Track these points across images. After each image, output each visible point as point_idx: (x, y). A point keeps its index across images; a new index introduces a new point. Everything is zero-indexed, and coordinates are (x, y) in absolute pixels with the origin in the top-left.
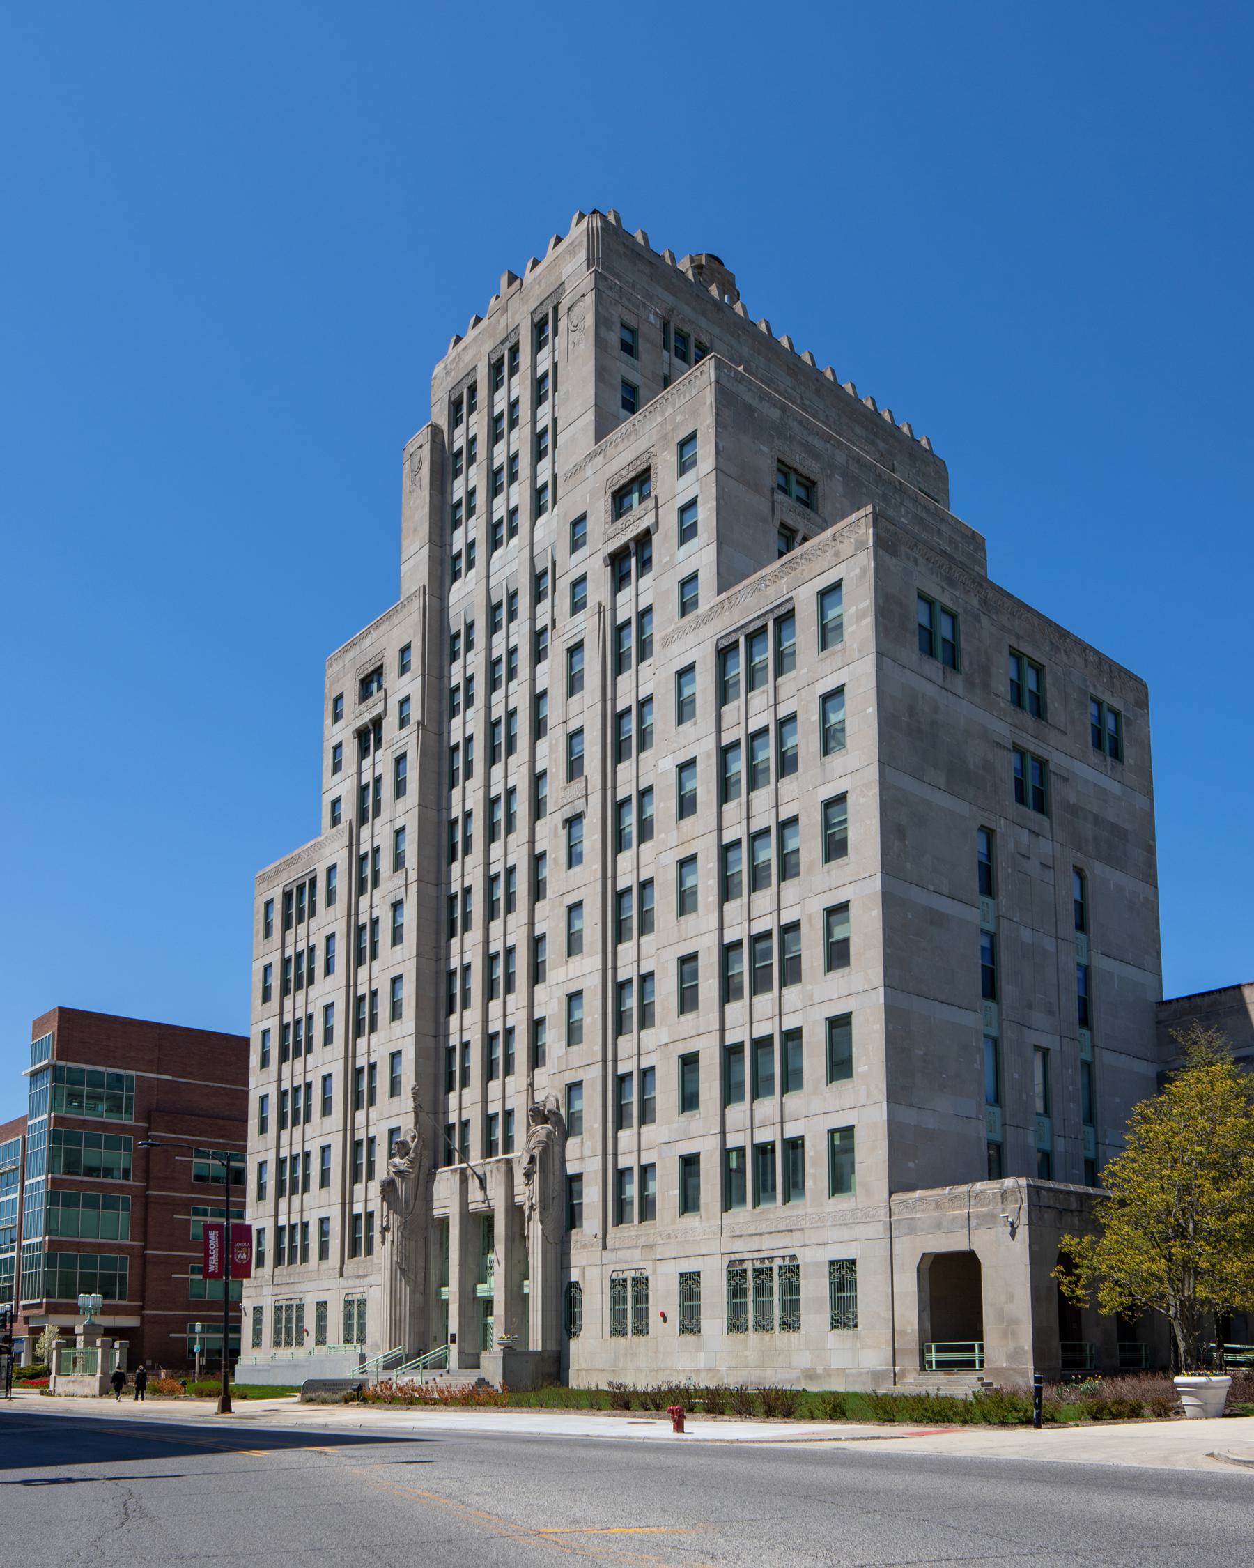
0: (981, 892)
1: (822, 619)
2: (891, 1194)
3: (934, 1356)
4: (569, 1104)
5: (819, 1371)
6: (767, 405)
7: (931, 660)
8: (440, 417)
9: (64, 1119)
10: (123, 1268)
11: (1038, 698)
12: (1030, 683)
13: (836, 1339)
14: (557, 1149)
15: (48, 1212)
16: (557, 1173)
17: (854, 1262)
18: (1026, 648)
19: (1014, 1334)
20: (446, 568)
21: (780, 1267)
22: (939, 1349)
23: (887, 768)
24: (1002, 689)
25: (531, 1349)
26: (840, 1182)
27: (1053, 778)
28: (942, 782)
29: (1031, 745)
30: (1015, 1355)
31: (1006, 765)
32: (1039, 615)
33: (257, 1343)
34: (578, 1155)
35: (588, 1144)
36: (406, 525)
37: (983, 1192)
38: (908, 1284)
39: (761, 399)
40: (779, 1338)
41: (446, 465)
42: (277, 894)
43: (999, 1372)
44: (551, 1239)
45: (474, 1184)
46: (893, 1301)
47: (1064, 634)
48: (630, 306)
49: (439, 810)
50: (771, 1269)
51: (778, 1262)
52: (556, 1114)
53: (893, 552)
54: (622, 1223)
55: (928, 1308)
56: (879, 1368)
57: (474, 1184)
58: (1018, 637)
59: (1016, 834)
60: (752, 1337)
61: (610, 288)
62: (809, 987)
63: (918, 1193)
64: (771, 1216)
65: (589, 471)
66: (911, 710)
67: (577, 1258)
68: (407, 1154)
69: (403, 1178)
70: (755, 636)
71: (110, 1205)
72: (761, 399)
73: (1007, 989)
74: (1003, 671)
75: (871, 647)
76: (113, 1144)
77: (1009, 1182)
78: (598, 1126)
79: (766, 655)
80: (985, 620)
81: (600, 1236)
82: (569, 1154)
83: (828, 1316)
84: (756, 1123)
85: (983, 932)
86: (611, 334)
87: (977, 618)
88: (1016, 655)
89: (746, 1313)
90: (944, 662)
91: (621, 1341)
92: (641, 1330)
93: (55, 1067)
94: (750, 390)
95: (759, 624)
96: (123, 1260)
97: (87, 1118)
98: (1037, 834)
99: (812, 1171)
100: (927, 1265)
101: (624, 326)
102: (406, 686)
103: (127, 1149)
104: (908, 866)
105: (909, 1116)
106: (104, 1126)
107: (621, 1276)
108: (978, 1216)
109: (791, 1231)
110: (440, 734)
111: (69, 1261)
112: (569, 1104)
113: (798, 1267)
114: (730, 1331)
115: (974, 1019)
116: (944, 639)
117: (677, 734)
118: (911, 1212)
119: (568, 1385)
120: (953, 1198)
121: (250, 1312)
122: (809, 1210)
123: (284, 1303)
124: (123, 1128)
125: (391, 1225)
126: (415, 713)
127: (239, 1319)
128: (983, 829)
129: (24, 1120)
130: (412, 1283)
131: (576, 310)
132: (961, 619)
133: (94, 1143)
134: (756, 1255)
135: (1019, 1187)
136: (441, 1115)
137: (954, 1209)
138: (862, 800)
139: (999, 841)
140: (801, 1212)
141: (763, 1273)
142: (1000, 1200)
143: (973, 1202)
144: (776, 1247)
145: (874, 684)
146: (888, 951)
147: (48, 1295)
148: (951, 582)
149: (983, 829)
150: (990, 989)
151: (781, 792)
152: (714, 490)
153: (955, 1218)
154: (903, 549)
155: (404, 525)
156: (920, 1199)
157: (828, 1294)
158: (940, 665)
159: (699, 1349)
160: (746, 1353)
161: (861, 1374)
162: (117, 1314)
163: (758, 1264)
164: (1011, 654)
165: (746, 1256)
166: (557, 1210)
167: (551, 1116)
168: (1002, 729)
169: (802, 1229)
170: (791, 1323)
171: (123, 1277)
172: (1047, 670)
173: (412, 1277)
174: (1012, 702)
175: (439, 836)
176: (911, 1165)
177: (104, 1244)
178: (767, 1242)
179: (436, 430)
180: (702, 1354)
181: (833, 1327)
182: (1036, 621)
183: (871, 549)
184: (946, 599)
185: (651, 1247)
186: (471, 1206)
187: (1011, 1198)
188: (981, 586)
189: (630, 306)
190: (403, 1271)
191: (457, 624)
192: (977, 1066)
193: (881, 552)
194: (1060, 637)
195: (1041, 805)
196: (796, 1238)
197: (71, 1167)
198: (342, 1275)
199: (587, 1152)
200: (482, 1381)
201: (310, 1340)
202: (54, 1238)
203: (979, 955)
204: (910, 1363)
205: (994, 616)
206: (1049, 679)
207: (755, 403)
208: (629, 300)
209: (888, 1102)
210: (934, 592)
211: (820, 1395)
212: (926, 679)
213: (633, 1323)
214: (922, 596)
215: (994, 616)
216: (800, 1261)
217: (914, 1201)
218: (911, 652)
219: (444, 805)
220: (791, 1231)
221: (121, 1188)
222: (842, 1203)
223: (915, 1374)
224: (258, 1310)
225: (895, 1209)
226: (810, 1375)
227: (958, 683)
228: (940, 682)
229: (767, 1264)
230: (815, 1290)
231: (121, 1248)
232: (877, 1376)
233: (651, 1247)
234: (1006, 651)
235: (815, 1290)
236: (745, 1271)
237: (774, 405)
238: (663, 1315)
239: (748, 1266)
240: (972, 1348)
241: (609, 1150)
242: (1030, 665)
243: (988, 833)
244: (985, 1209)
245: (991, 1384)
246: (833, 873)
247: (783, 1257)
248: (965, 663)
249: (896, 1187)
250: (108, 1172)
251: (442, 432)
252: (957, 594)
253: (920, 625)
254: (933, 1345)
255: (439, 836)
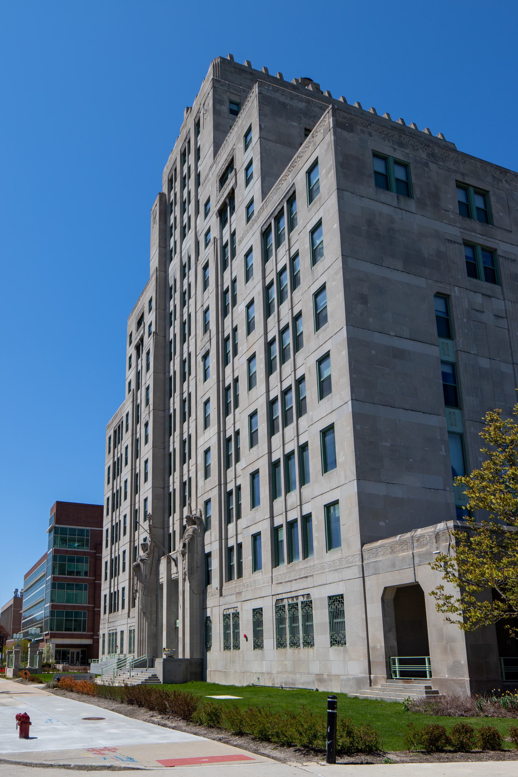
0: (440, 335)
1: (310, 185)
2: (362, 545)
3: (397, 667)
4: (206, 513)
5: (325, 677)
6: (296, 101)
7: (387, 192)
8: (165, 190)
9: (58, 550)
10: (84, 617)
11: (485, 212)
12: (478, 202)
13: (334, 652)
14: (199, 539)
15: (52, 592)
16: (200, 553)
17: (342, 596)
18: (468, 180)
19: (452, 651)
20: (166, 256)
21: (302, 602)
22: (401, 662)
23: (349, 260)
24: (451, 207)
25: (186, 658)
26: (332, 541)
27: (501, 260)
28: (399, 265)
29: (480, 240)
30: (454, 668)
31: (459, 256)
32: (481, 161)
33: (103, 653)
34: (209, 542)
35: (213, 534)
36: (152, 243)
37: (422, 536)
38: (376, 611)
39: (292, 99)
40: (303, 652)
41: (166, 209)
42: (112, 433)
43: (442, 682)
44: (195, 592)
45: (173, 564)
46: (368, 624)
47: (504, 171)
48: (235, 92)
49: (165, 374)
50: (297, 604)
51: (301, 599)
52: (200, 519)
53: (350, 129)
54: (231, 580)
55: (394, 630)
56: (360, 675)
57: (173, 564)
58: (463, 174)
59: (467, 297)
60: (289, 650)
61: (222, 85)
62: (311, 413)
63: (380, 542)
64: (297, 568)
65: (210, 175)
66: (370, 223)
67: (210, 602)
68: (147, 550)
69: (144, 563)
70: (278, 218)
71: (79, 587)
72: (292, 99)
73: (468, 400)
74: (452, 197)
75: (335, 187)
76: (79, 560)
77: (441, 526)
78: (217, 523)
79: (285, 222)
80: (433, 167)
81: (219, 588)
82: (206, 541)
83: (328, 636)
84: (289, 508)
85: (443, 362)
86: (223, 107)
87: (426, 165)
88: (462, 186)
89: (286, 635)
90: (398, 192)
91: (227, 652)
92: (237, 647)
93: (55, 527)
94: (283, 95)
95: (280, 207)
96: (85, 613)
97: (69, 549)
98: (489, 297)
99: (317, 535)
100: (391, 596)
101: (231, 102)
102: (150, 318)
103: (87, 562)
104: (371, 320)
105: (380, 489)
106: (76, 553)
107: (228, 613)
108: (420, 555)
109: (306, 577)
110: (165, 337)
111: (60, 614)
112: (206, 513)
113: (311, 601)
114: (278, 647)
115: (440, 421)
116: (397, 180)
117: (246, 288)
118: (375, 557)
119: (206, 681)
120: (402, 543)
121: (101, 636)
122: (316, 562)
123: (111, 632)
124: (85, 553)
125: (138, 589)
126: (153, 329)
127: (98, 639)
128: (438, 295)
129: (47, 553)
130: (149, 620)
131: (206, 103)
132: (412, 167)
133: (71, 560)
134: (289, 595)
135: (448, 528)
136: (166, 529)
137: (403, 551)
138: (334, 283)
139: (454, 301)
140: (311, 564)
141: (293, 607)
142: (434, 541)
143: (415, 544)
144: (298, 588)
145: (337, 208)
146: (355, 376)
147: (51, 630)
148: (401, 145)
149: (438, 295)
150: (452, 397)
151: (294, 299)
152: (259, 149)
153: (404, 558)
154: (359, 128)
155: (151, 243)
156: (380, 547)
157: (328, 621)
158: (394, 195)
159: (263, 659)
160: (286, 662)
161: (349, 680)
162: (81, 638)
163: (290, 601)
164: (458, 186)
165: (284, 596)
166: (199, 575)
167: (196, 520)
168: (454, 230)
169: (312, 576)
170: (309, 643)
171: (85, 621)
172: (491, 193)
173: (149, 616)
174: (461, 214)
175: (165, 386)
176: (382, 524)
177: (76, 606)
178: (295, 586)
179: (162, 195)
180: (264, 662)
181: (332, 644)
182: (479, 164)
183: (332, 130)
184: (399, 155)
185: (240, 593)
186: (173, 576)
187: (443, 538)
188: (429, 146)
189: (235, 92)
190: (144, 613)
191: (171, 282)
192: (443, 453)
193: (339, 130)
194: (501, 173)
195: (492, 277)
196: (308, 583)
197: (62, 572)
198: (129, 617)
199: (213, 539)
200: (155, 676)
201: (322, 635)
202: (53, 603)
203: (441, 377)
204: (380, 672)
205: (441, 163)
206: (493, 199)
207: (287, 101)
208: (234, 89)
209: (358, 479)
210: (386, 149)
211: (324, 693)
212: (383, 205)
213: (290, 638)
214: (376, 155)
215: (441, 163)
216: (313, 598)
217: (377, 548)
218: (369, 188)
219: (167, 370)
220: (306, 577)
221: (83, 580)
222: (335, 554)
223: (383, 682)
224: (104, 635)
225: (366, 556)
226: (320, 679)
227: (412, 205)
228: (395, 204)
229: (295, 601)
230: (321, 616)
231: (83, 608)
232: (359, 682)
233: (240, 593)
234: (453, 184)
235: (321, 616)
236: (284, 606)
237: (302, 101)
238: (245, 636)
239: (285, 602)
240: (423, 662)
241: (223, 537)
242: (476, 193)
243: (445, 297)
244: (424, 549)
245: (437, 692)
246: (320, 337)
247: (303, 595)
248: (417, 192)
249: (366, 538)
250: (78, 573)
251: (166, 195)
252: (408, 151)
253: (376, 173)
254: (396, 658)
255: (165, 386)
